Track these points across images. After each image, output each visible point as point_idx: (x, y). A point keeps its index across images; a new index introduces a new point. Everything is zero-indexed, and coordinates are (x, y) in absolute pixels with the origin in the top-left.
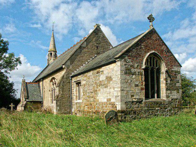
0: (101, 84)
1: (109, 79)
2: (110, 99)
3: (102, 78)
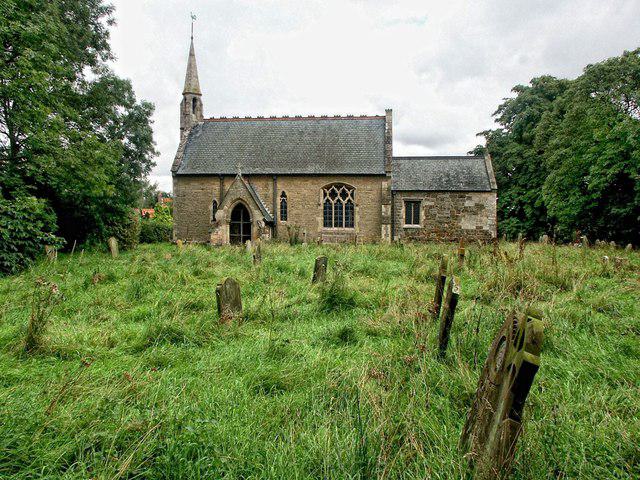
0: (466, 210)
1: (480, 207)
2: (481, 227)
3: (468, 203)
